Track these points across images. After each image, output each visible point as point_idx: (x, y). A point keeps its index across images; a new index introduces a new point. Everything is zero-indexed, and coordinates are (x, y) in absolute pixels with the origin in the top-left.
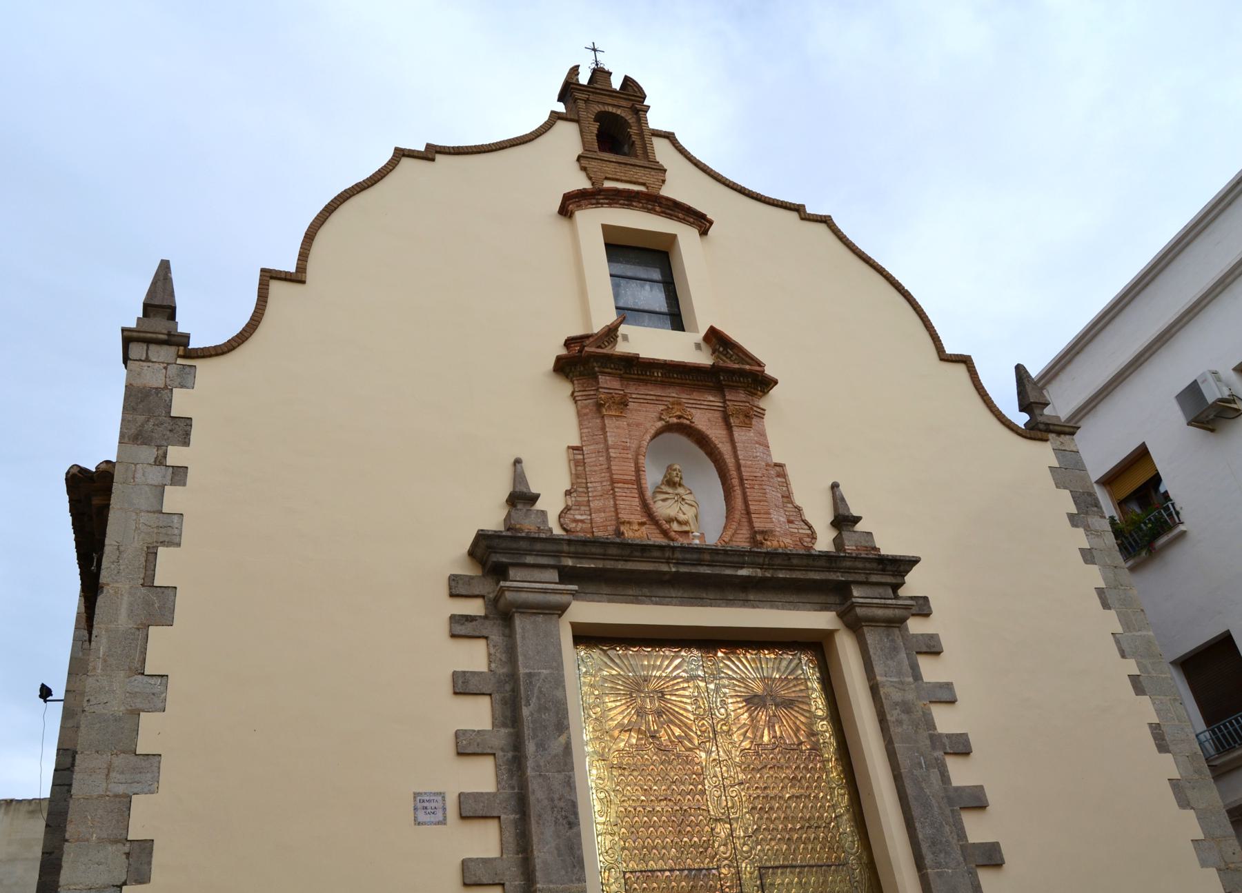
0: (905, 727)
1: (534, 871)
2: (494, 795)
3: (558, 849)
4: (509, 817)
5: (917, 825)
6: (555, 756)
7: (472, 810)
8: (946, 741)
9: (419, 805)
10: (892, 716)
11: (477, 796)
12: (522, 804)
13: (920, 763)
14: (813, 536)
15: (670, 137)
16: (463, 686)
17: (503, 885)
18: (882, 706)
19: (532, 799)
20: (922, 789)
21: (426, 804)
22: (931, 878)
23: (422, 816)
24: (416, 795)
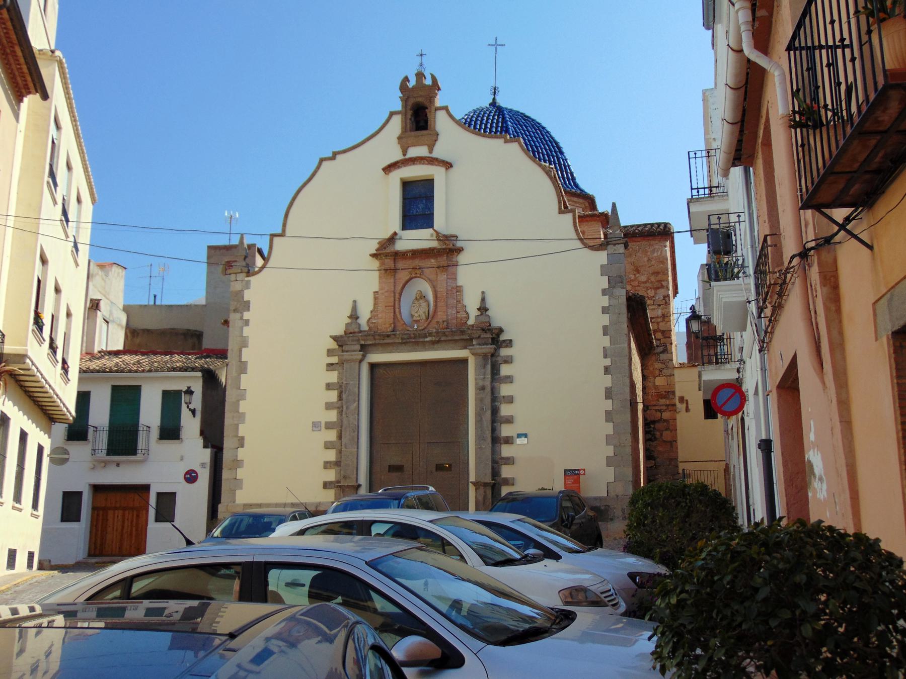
7: (329, 426)
11: (331, 442)
14: (468, 318)
15: (446, 108)
16: (329, 387)
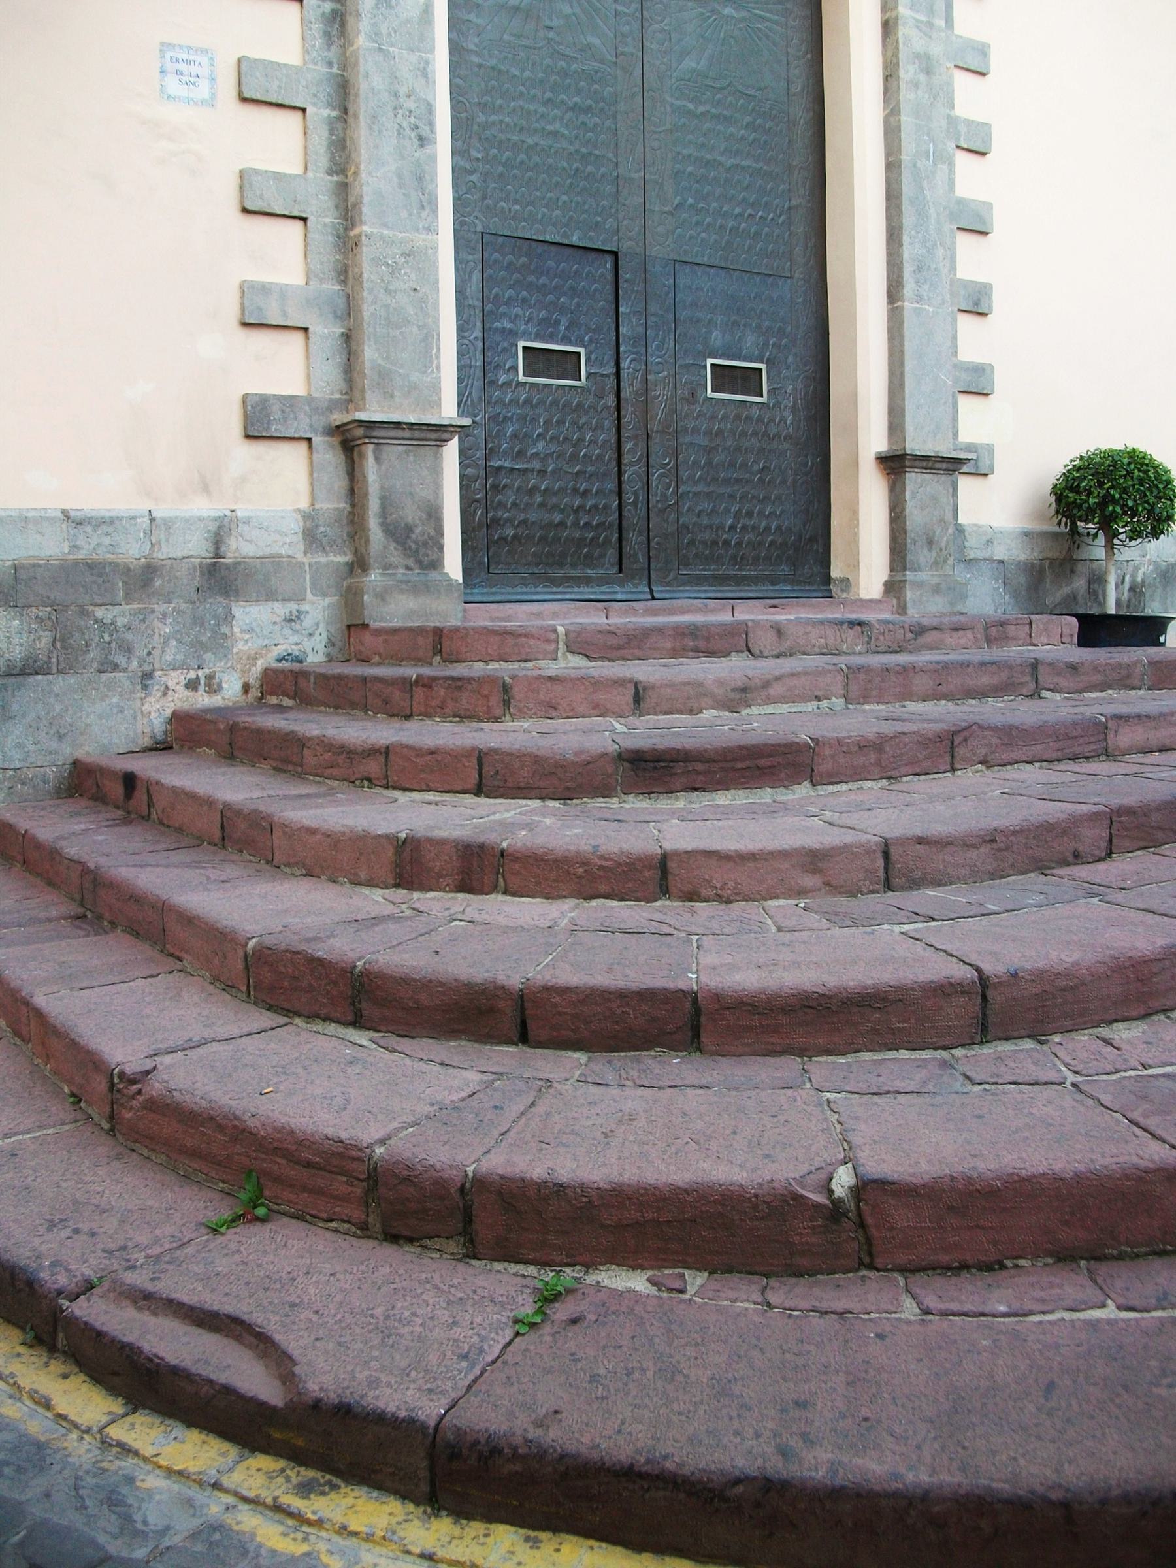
0: (920, 93)
1: (357, 205)
2: (298, 70)
3: (400, 176)
4: (320, 113)
5: (906, 239)
6: (408, 21)
8: (963, 129)
9: (169, 66)
10: (907, 72)
12: (343, 94)
13: (928, 152)
17: (304, 110)
18: (896, 55)
19: (363, 86)
20: (922, 189)
21: (181, 66)
22: (906, 314)
23: (173, 85)
24: (165, 46)
